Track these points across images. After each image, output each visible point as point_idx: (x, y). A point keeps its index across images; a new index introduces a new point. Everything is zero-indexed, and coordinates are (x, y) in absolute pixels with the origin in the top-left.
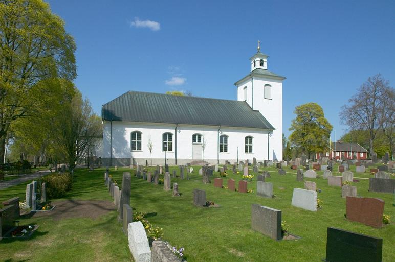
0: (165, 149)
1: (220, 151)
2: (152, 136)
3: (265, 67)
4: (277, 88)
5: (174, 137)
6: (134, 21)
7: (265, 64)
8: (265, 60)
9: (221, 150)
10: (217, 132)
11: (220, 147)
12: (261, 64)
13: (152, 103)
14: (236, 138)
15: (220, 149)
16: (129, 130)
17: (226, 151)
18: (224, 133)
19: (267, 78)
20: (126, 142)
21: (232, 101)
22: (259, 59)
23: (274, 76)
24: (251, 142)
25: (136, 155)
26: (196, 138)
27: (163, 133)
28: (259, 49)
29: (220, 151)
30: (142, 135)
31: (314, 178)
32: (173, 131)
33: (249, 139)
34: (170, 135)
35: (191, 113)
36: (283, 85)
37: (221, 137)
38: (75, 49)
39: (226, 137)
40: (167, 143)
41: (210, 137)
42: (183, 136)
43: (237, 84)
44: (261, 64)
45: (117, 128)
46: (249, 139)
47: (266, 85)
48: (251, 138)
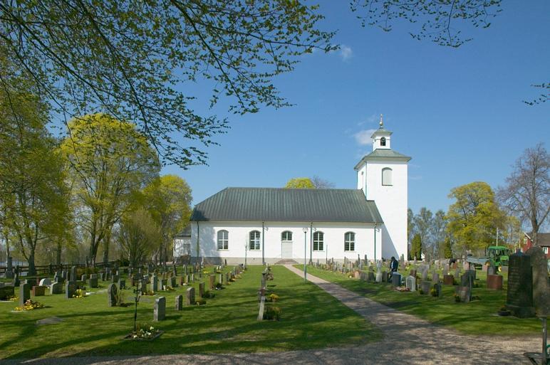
0: (347, 248)
1: (314, 249)
2: (238, 235)
3: (388, 146)
4: (400, 172)
5: (261, 234)
6: (114, 67)
7: (388, 143)
8: (387, 138)
9: (315, 248)
10: (373, 230)
11: (314, 245)
12: (383, 143)
13: (247, 200)
14: (334, 236)
15: (314, 247)
16: (217, 229)
17: (321, 248)
18: (318, 229)
19: (372, 160)
20: (214, 243)
21: (352, 191)
22: (380, 138)
23: (398, 157)
24: (353, 238)
25: (223, 254)
26: (287, 236)
27: (250, 231)
28: (381, 125)
29: (314, 249)
30: (356, 236)
31: (204, 289)
32: (260, 229)
33: (350, 236)
34: (258, 233)
35: (285, 208)
36: (410, 173)
37: (316, 234)
38: (186, 136)
39: (353, 234)
40: (318, 243)
41: (302, 235)
42: (272, 234)
43: (357, 168)
44: (383, 143)
45: (205, 228)
46: (350, 236)
47: (384, 169)
48: (353, 234)
